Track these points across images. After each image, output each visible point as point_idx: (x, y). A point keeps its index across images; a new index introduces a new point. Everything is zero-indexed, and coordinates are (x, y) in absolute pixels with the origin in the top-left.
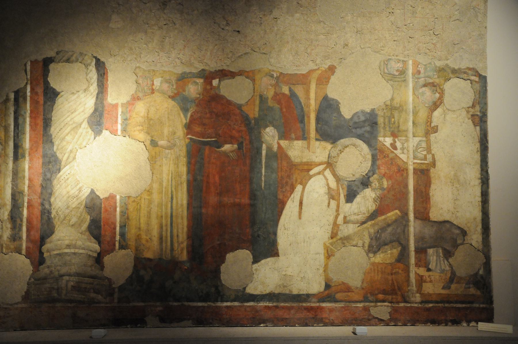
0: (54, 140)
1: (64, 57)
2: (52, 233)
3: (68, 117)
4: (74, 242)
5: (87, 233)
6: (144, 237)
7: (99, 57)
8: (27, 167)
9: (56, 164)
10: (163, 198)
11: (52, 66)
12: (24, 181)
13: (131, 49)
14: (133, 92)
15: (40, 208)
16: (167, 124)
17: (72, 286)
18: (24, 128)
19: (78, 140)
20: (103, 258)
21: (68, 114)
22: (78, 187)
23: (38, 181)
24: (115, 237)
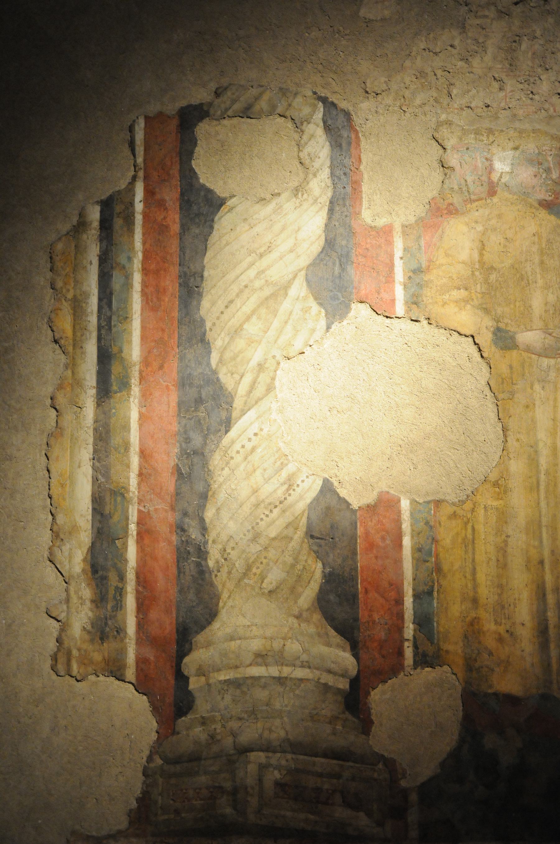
0: (210, 336)
1: (234, 101)
2: (212, 615)
3: (248, 268)
4: (277, 645)
5: (317, 617)
6: (490, 626)
7: (332, 98)
8: (134, 415)
9: (219, 406)
10: (543, 504)
11: (203, 129)
12: (128, 458)
13: (421, 74)
14: (435, 193)
15: (174, 538)
16: (540, 282)
17: (277, 784)
18: (126, 301)
19: (280, 331)
20: (368, 693)
21: (250, 259)
22: (284, 474)
23: (167, 458)
24: (400, 629)
